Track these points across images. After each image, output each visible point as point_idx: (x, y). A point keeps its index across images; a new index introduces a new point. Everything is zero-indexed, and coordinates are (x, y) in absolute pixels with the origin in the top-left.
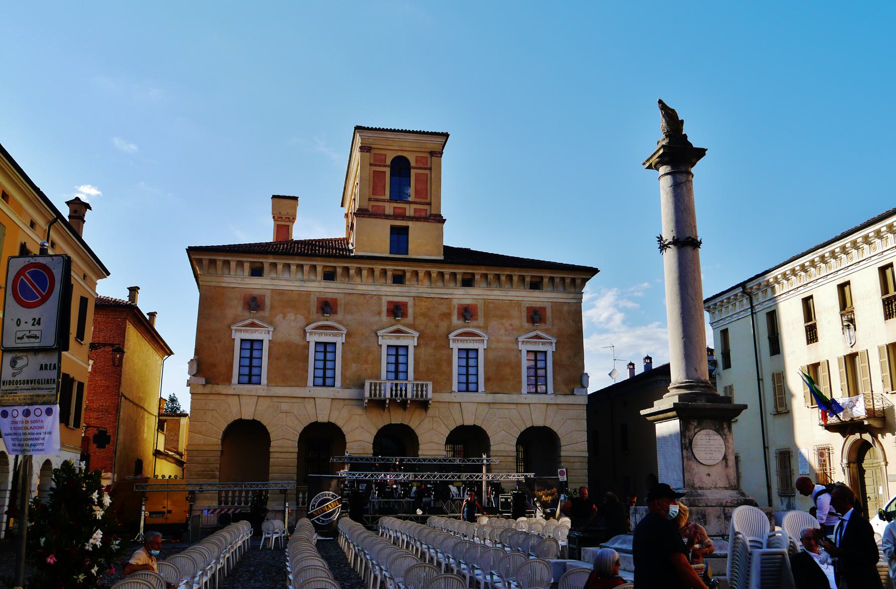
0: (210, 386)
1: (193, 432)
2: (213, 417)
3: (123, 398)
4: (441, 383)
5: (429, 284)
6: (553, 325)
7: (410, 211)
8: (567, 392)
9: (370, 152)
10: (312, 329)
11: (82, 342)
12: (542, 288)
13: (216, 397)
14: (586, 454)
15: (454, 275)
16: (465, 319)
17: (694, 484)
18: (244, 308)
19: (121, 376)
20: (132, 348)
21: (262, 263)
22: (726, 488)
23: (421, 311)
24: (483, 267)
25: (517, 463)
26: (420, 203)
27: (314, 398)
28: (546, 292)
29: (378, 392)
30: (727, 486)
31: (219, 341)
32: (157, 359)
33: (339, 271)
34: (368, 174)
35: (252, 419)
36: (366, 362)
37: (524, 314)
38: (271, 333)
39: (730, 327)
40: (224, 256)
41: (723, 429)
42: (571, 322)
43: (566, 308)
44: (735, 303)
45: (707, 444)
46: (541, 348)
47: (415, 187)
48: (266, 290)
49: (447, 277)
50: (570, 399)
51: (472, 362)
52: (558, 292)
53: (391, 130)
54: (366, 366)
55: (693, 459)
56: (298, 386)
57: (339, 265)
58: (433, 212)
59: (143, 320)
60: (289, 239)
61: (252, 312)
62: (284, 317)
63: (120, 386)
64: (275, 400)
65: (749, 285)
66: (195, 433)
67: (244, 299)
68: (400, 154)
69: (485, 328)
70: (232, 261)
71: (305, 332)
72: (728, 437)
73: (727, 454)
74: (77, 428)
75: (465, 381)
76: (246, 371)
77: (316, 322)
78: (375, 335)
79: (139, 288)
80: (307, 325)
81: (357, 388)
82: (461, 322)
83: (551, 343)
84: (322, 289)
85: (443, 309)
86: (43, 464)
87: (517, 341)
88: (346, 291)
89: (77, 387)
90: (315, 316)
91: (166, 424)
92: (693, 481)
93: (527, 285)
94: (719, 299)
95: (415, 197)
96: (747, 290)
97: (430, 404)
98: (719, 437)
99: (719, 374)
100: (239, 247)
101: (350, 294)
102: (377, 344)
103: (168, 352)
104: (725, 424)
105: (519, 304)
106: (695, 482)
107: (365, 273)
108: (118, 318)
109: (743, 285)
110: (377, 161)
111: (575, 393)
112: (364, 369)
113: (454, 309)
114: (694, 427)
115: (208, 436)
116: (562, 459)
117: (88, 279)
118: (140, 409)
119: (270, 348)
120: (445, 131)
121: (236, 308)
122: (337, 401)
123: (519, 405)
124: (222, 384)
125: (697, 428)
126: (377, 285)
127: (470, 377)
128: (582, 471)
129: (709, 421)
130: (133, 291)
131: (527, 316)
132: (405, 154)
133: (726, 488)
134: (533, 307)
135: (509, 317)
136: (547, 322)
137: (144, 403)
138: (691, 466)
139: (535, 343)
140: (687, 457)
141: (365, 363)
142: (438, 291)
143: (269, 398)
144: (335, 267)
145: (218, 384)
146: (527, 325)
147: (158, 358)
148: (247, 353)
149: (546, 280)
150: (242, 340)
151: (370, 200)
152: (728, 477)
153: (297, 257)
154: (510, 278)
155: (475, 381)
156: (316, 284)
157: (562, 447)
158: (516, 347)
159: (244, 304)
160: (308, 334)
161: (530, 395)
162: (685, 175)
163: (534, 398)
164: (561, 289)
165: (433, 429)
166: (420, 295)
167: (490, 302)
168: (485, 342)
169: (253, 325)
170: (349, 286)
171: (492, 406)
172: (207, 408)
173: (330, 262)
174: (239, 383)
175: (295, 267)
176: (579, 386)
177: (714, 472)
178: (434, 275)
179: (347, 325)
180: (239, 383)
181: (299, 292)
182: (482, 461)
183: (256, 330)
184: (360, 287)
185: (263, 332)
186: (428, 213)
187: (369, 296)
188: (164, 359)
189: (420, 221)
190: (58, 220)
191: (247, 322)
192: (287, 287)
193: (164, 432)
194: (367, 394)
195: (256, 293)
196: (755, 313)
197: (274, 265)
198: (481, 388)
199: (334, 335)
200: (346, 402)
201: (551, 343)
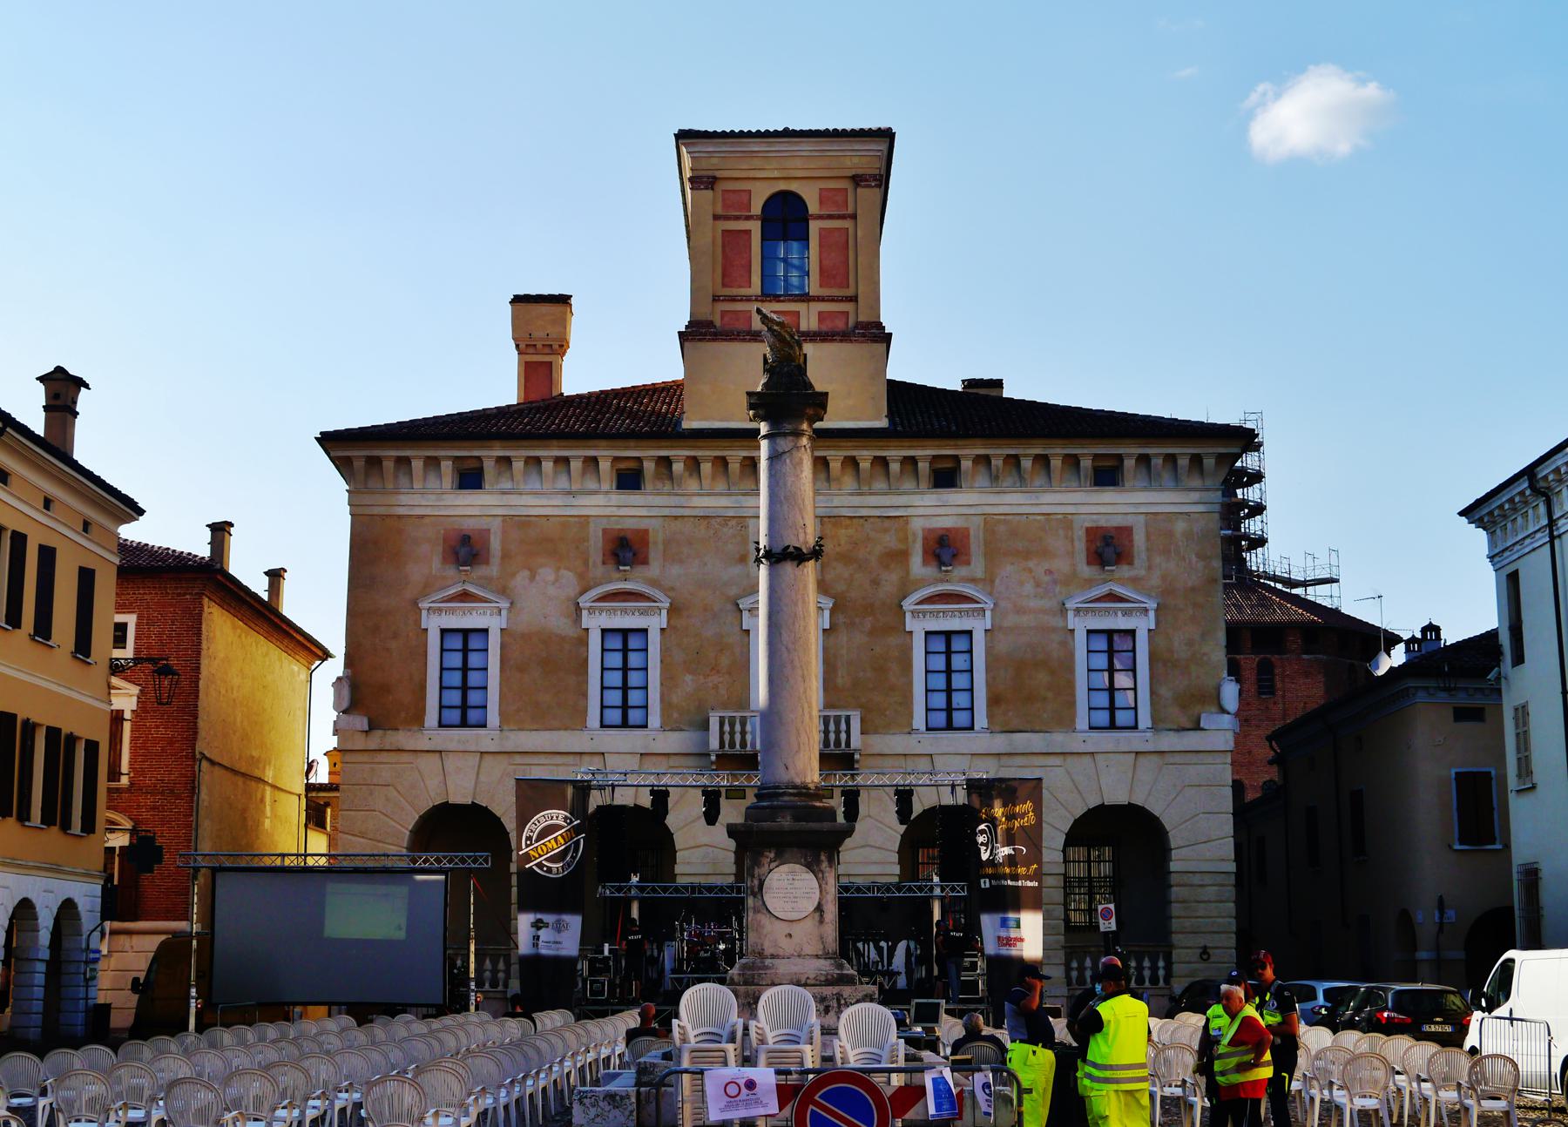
0: (379, 733)
1: (347, 834)
2: (388, 800)
3: (205, 764)
4: (887, 713)
5: (855, 486)
6: (1150, 568)
7: (809, 318)
8: (1185, 722)
9: (713, 189)
10: (593, 602)
11: (88, 660)
12: (1123, 480)
13: (393, 757)
14: (1232, 867)
15: (910, 462)
16: (941, 563)
17: (763, 949)
18: (445, 560)
19: (197, 718)
20: (221, 655)
21: (479, 458)
22: (817, 955)
23: (838, 549)
24: (978, 441)
25: (1065, 888)
26: (832, 299)
27: (603, 754)
28: (1133, 489)
29: (738, 737)
30: (820, 953)
31: (395, 636)
32: (293, 670)
33: (649, 466)
34: (709, 240)
35: (1127, 803)
36: (715, 669)
37: (1080, 546)
38: (504, 613)
39: (1519, 565)
40: (397, 448)
41: (819, 862)
42: (1194, 559)
43: (1180, 526)
44: (1527, 512)
45: (789, 887)
46: (1122, 623)
47: (821, 261)
48: (491, 518)
49: (895, 467)
50: (1191, 740)
51: (959, 662)
52: (1162, 489)
53: (759, 134)
54: (715, 679)
55: (765, 911)
56: (566, 729)
57: (648, 454)
58: (861, 318)
59: (242, 594)
60: (554, 394)
61: (461, 568)
62: (532, 578)
63: (195, 739)
64: (518, 759)
65: (1542, 472)
66: (353, 835)
67: (445, 540)
68: (783, 186)
69: (988, 581)
70: (415, 457)
71: (578, 609)
72: (827, 874)
73: (823, 902)
74: (88, 834)
76: (454, 697)
77: (602, 584)
78: (734, 608)
79: (232, 525)
80: (583, 592)
81: (699, 730)
82: (930, 571)
83: (1146, 610)
84: (615, 509)
85: (890, 541)
86: (14, 909)
87: (1063, 610)
88: (666, 512)
89: (85, 750)
90: (598, 570)
91: (329, 811)
92: (762, 945)
93: (1086, 477)
94: (1504, 497)
95: (821, 286)
96: (1538, 481)
97: (858, 761)
98: (811, 876)
99: (1506, 678)
100: (434, 424)
101: (676, 517)
102: (739, 629)
103: (320, 653)
104: (822, 853)
105: (1066, 522)
106: (765, 947)
107: (706, 468)
108: (185, 594)
109: (1529, 472)
110: (734, 206)
111: (1202, 725)
112: (710, 685)
113: (914, 541)
114: (769, 860)
115: (379, 841)
116: (1174, 879)
117: (93, 529)
118: (253, 784)
119: (503, 646)
120: (884, 125)
121: (427, 562)
122: (654, 759)
123: (1069, 759)
124: (403, 730)
125: (774, 861)
126: (737, 495)
127: (954, 695)
128: (1221, 905)
129: (795, 849)
130: (220, 531)
131: (1088, 550)
132: (794, 187)
133: (817, 957)
134: (1102, 528)
135: (1045, 553)
136: (1136, 562)
137: (264, 768)
138: (760, 921)
139: (1107, 610)
140: (754, 908)
141: (714, 672)
142: (878, 501)
143: (506, 756)
144: (639, 460)
145: (398, 730)
146: (1086, 571)
147: (296, 668)
148: (455, 660)
149: (1129, 463)
150: (444, 632)
151: (716, 299)
152: (822, 938)
153: (555, 442)
154: (1043, 461)
155: (967, 705)
156: (599, 500)
157: (1173, 852)
158: (1061, 624)
159: (444, 551)
160: (585, 613)
161: (1095, 735)
162: (791, 438)
163: (1107, 740)
164: (1167, 476)
165: (869, 816)
166: (836, 512)
167: (999, 521)
168: (988, 613)
169: (465, 596)
170: (673, 501)
171: (1004, 760)
172: (375, 781)
173: (627, 448)
174: (441, 725)
175: (552, 463)
176: (1214, 709)
177: (796, 930)
178: (865, 465)
179: (672, 589)
180: (441, 725)
181: (563, 519)
182: (931, 889)
183: (473, 608)
184: (697, 501)
185: (489, 612)
186: (851, 322)
187: (718, 520)
188: (313, 667)
189: (832, 341)
190: (8, 429)
191: (452, 591)
192: (537, 509)
193: (325, 829)
194: (714, 744)
195: (469, 525)
196: (1559, 536)
197: (507, 461)
198: (981, 720)
199: (643, 612)
200: (673, 761)
201: (1146, 610)
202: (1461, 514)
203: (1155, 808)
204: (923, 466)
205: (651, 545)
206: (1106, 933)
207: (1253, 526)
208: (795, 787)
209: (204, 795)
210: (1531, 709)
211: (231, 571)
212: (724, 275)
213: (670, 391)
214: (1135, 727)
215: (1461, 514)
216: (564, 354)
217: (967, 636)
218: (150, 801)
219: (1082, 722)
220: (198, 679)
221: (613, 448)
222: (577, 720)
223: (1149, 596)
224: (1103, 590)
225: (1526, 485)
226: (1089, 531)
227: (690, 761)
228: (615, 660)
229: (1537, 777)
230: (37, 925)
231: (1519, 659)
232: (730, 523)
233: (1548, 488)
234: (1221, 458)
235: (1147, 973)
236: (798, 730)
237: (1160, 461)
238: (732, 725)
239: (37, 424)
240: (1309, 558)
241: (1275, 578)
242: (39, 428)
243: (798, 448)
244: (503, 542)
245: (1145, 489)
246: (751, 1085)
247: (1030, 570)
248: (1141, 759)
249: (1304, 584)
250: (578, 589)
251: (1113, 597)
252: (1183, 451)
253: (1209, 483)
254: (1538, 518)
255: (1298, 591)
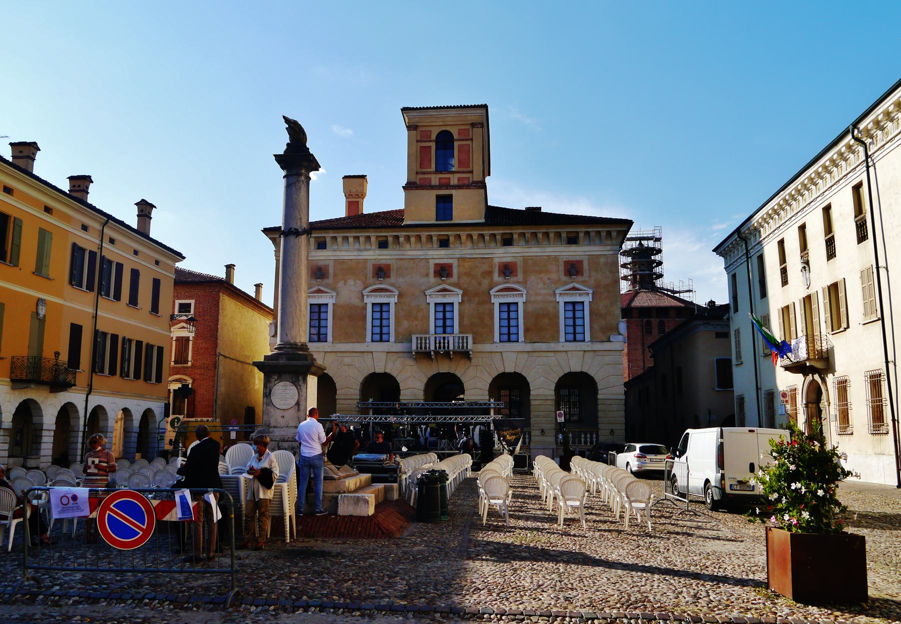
3: (221, 357)
5: (472, 246)
6: (590, 277)
14: (623, 397)
21: (324, 237)
23: (465, 271)
24: (520, 227)
28: (584, 245)
29: (423, 345)
33: (390, 239)
36: (416, 319)
37: (562, 268)
41: (298, 381)
42: (608, 273)
43: (602, 260)
46: (578, 299)
49: (487, 238)
50: (607, 346)
52: (595, 244)
54: (416, 322)
58: (475, 179)
60: (360, 213)
62: (345, 284)
63: (216, 347)
64: (339, 354)
65: (743, 229)
67: (312, 269)
68: (444, 128)
69: (524, 283)
71: (363, 296)
75: (322, 321)
80: (364, 289)
82: (501, 279)
83: (588, 294)
85: (486, 267)
87: (555, 294)
90: (371, 280)
94: (729, 242)
98: (294, 388)
101: (401, 259)
105: (556, 259)
107: (413, 239)
109: (738, 231)
113: (495, 267)
116: (599, 402)
120: (483, 103)
122: (391, 354)
123: (557, 353)
130: (230, 268)
131: (565, 269)
132: (448, 128)
136: (584, 274)
139: (572, 294)
144: (386, 237)
146: (564, 278)
149: (581, 235)
151: (417, 173)
154: (547, 235)
156: (371, 253)
158: (554, 299)
160: (365, 297)
161: (568, 344)
162: (295, 177)
164: (597, 241)
166: (464, 256)
168: (524, 296)
169: (319, 291)
173: (382, 232)
178: (475, 237)
179: (400, 287)
182: (490, 405)
184: (409, 253)
189: (463, 189)
190: (110, 221)
191: (314, 289)
194: (414, 348)
195: (321, 263)
196: (751, 257)
197: (335, 238)
198: (521, 338)
199: (388, 296)
200: (399, 355)
201: (588, 294)
202: (713, 251)
203: (592, 373)
204: (498, 237)
205: (391, 271)
206: (560, 423)
207: (658, 270)
208: (290, 344)
209: (221, 368)
210: (741, 331)
211: (235, 284)
212: (421, 164)
213: (400, 212)
214: (584, 341)
215: (713, 251)
216: (364, 197)
217: (582, 304)
218: (198, 371)
219: (562, 339)
220: (218, 324)
221: (377, 232)
222: (362, 339)
223: (590, 288)
224: (571, 286)
225: (737, 236)
226: (565, 262)
227: (406, 355)
228: (377, 315)
229: (743, 359)
230: (78, 415)
231: (736, 310)
232: (422, 261)
233: (746, 237)
234: (619, 232)
235: (588, 440)
236: (293, 317)
237: (594, 234)
238: (421, 341)
239: (133, 222)
240: (681, 282)
241: (667, 290)
242: (135, 225)
243: (299, 182)
244: (334, 271)
245: (589, 245)
246: (75, 498)
247: (542, 278)
248: (586, 353)
249: (679, 292)
250: (363, 288)
251: (574, 289)
252: (603, 229)
253: (614, 242)
254: (742, 250)
255: (677, 295)
